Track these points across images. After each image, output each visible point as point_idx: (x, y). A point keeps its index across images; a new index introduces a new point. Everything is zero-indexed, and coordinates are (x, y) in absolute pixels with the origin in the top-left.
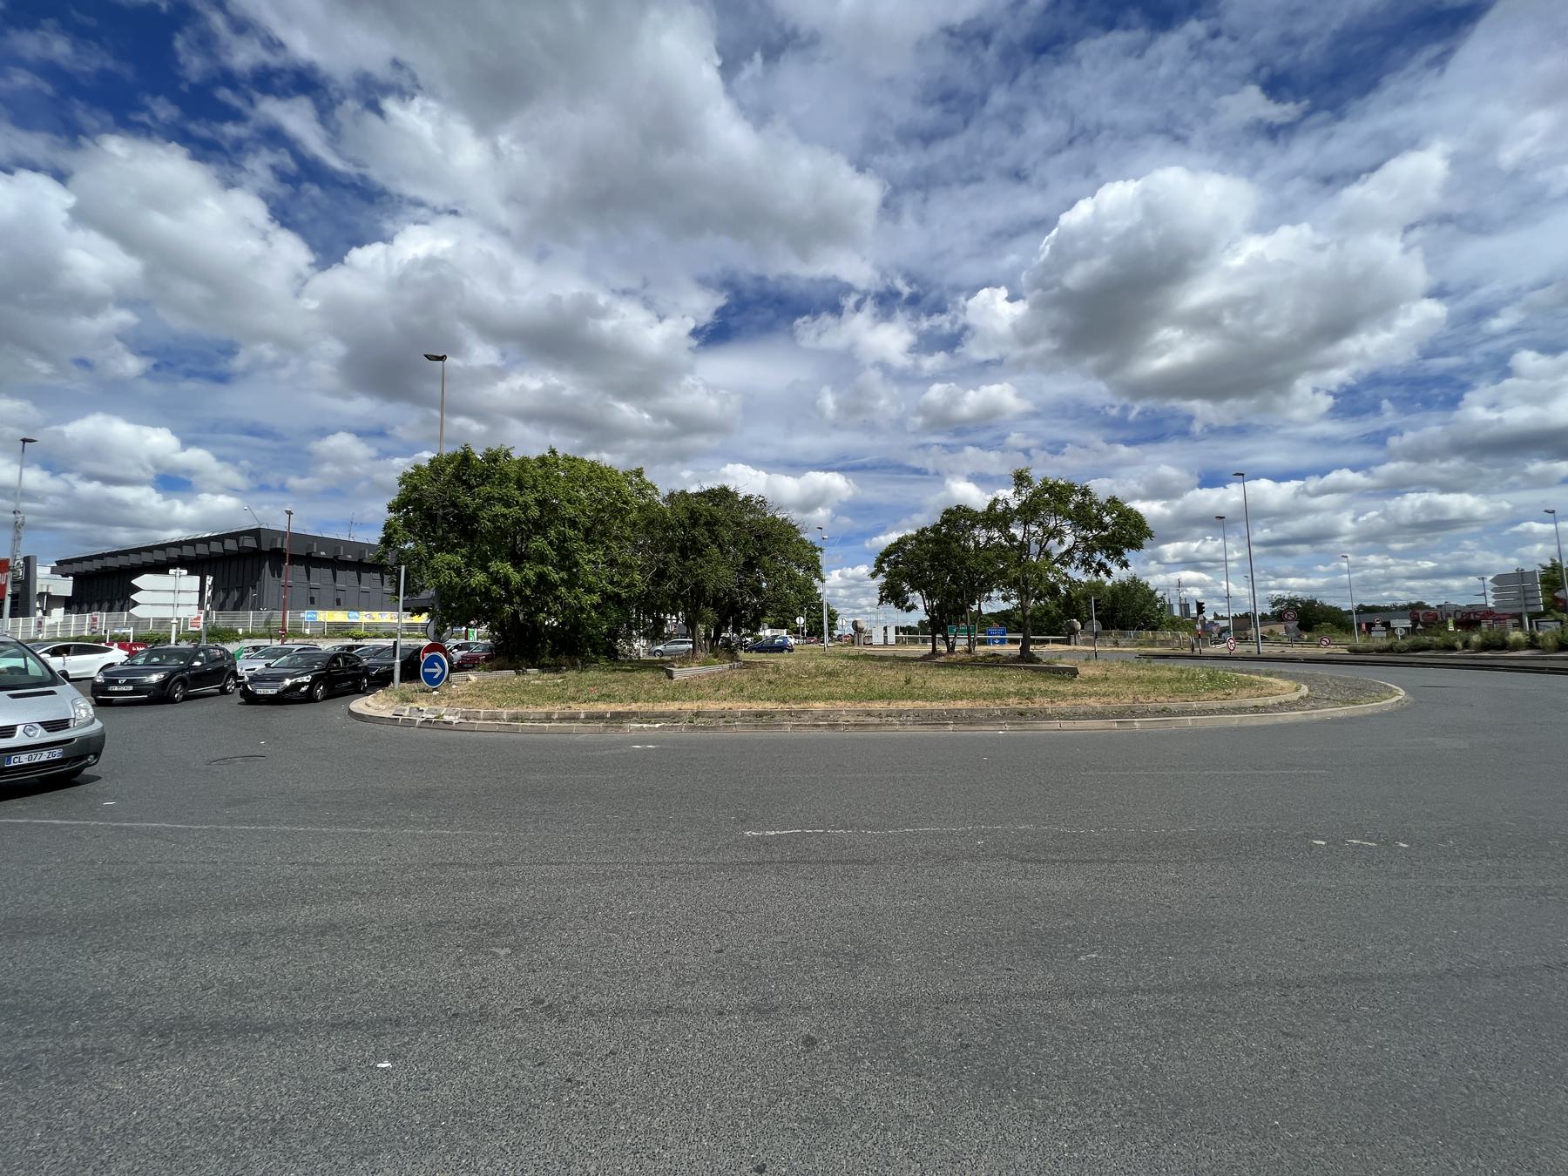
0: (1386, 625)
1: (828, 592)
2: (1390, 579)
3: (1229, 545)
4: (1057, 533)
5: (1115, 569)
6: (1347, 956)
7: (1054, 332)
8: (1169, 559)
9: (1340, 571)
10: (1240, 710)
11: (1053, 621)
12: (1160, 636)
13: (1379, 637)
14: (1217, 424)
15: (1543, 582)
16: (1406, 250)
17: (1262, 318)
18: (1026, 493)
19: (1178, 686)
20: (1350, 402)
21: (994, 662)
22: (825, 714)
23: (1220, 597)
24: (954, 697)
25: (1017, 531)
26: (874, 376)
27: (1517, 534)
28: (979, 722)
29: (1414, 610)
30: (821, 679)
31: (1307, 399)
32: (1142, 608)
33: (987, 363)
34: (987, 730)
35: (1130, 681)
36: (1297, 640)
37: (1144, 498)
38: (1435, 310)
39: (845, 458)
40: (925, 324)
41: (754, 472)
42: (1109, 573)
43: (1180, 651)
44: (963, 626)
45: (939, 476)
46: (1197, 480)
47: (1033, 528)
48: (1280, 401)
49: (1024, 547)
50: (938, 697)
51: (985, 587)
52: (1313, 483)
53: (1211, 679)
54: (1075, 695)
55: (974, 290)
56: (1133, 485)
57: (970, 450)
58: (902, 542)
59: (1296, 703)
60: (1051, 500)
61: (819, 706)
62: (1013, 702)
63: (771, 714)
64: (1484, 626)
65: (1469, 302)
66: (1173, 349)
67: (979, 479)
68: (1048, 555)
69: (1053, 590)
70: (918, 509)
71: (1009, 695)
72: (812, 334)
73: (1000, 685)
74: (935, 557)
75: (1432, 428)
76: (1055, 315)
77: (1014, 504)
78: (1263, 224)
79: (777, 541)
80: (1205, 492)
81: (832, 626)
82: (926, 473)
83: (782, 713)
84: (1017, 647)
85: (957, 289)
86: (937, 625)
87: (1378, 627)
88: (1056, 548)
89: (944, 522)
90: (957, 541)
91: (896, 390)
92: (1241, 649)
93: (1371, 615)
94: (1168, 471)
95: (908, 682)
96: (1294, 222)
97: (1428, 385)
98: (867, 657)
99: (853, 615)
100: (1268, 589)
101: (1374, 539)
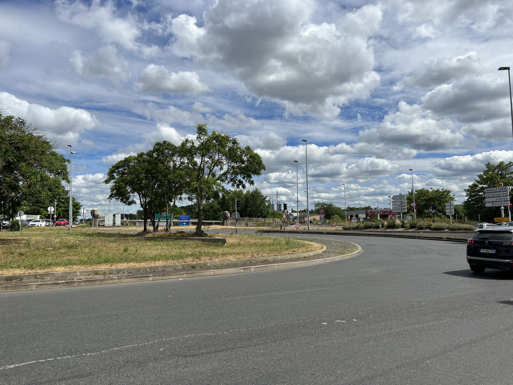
0: (357, 216)
1: (74, 190)
2: (359, 195)
3: (299, 175)
4: (218, 163)
5: (247, 185)
6: (331, 379)
7: (221, 48)
8: (272, 181)
9: (341, 191)
10: (298, 259)
11: (215, 212)
12: (268, 220)
13: (354, 223)
14: (295, 114)
15: (407, 199)
16: (368, 48)
17: (314, 65)
18: (204, 138)
19: (274, 247)
20: (347, 112)
21: (182, 236)
22: (64, 276)
23: (294, 201)
24: (155, 259)
25: (198, 160)
26: (112, 50)
27: (400, 178)
28: (169, 274)
29: (367, 209)
30: (63, 251)
31: (331, 107)
32: (260, 205)
33: (184, 59)
34: (173, 278)
35: (251, 245)
36: (324, 223)
37: (263, 148)
38: (376, 77)
39: (91, 101)
40: (146, 26)
41: (18, 101)
42: (244, 187)
43: (276, 229)
44: (164, 214)
45: (153, 122)
46: (286, 142)
47: (206, 159)
48: (320, 108)
49: (201, 169)
50: (145, 259)
51: (178, 191)
52: (332, 148)
53: (287, 244)
54: (223, 255)
55: (176, 14)
56: (257, 141)
57: (172, 109)
58: (127, 161)
59: (321, 254)
60: (215, 144)
61: (60, 270)
62: (189, 261)
63: (19, 278)
64: (389, 217)
65: (388, 77)
66: (277, 74)
67: (178, 126)
68: (214, 175)
69: (216, 195)
70: (139, 140)
71: (187, 256)
72: (68, 12)
73: (183, 251)
74: (148, 172)
75: (373, 130)
76: (221, 40)
77: (197, 144)
78: (317, 20)
79: (34, 152)
80: (289, 148)
81: (76, 213)
82: (145, 118)
83: (29, 276)
84: (195, 227)
85: (169, 9)
86: (148, 214)
87: (354, 217)
88: (218, 172)
89: (155, 150)
90: (163, 163)
91: (126, 63)
92: (302, 228)
93: (353, 212)
94: (273, 135)
95: (125, 250)
96: (329, 23)
97: (370, 110)
98: (99, 234)
99: (92, 206)
100: (314, 198)
101: (353, 176)
